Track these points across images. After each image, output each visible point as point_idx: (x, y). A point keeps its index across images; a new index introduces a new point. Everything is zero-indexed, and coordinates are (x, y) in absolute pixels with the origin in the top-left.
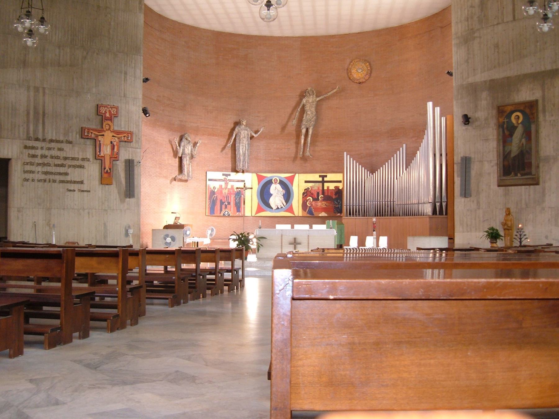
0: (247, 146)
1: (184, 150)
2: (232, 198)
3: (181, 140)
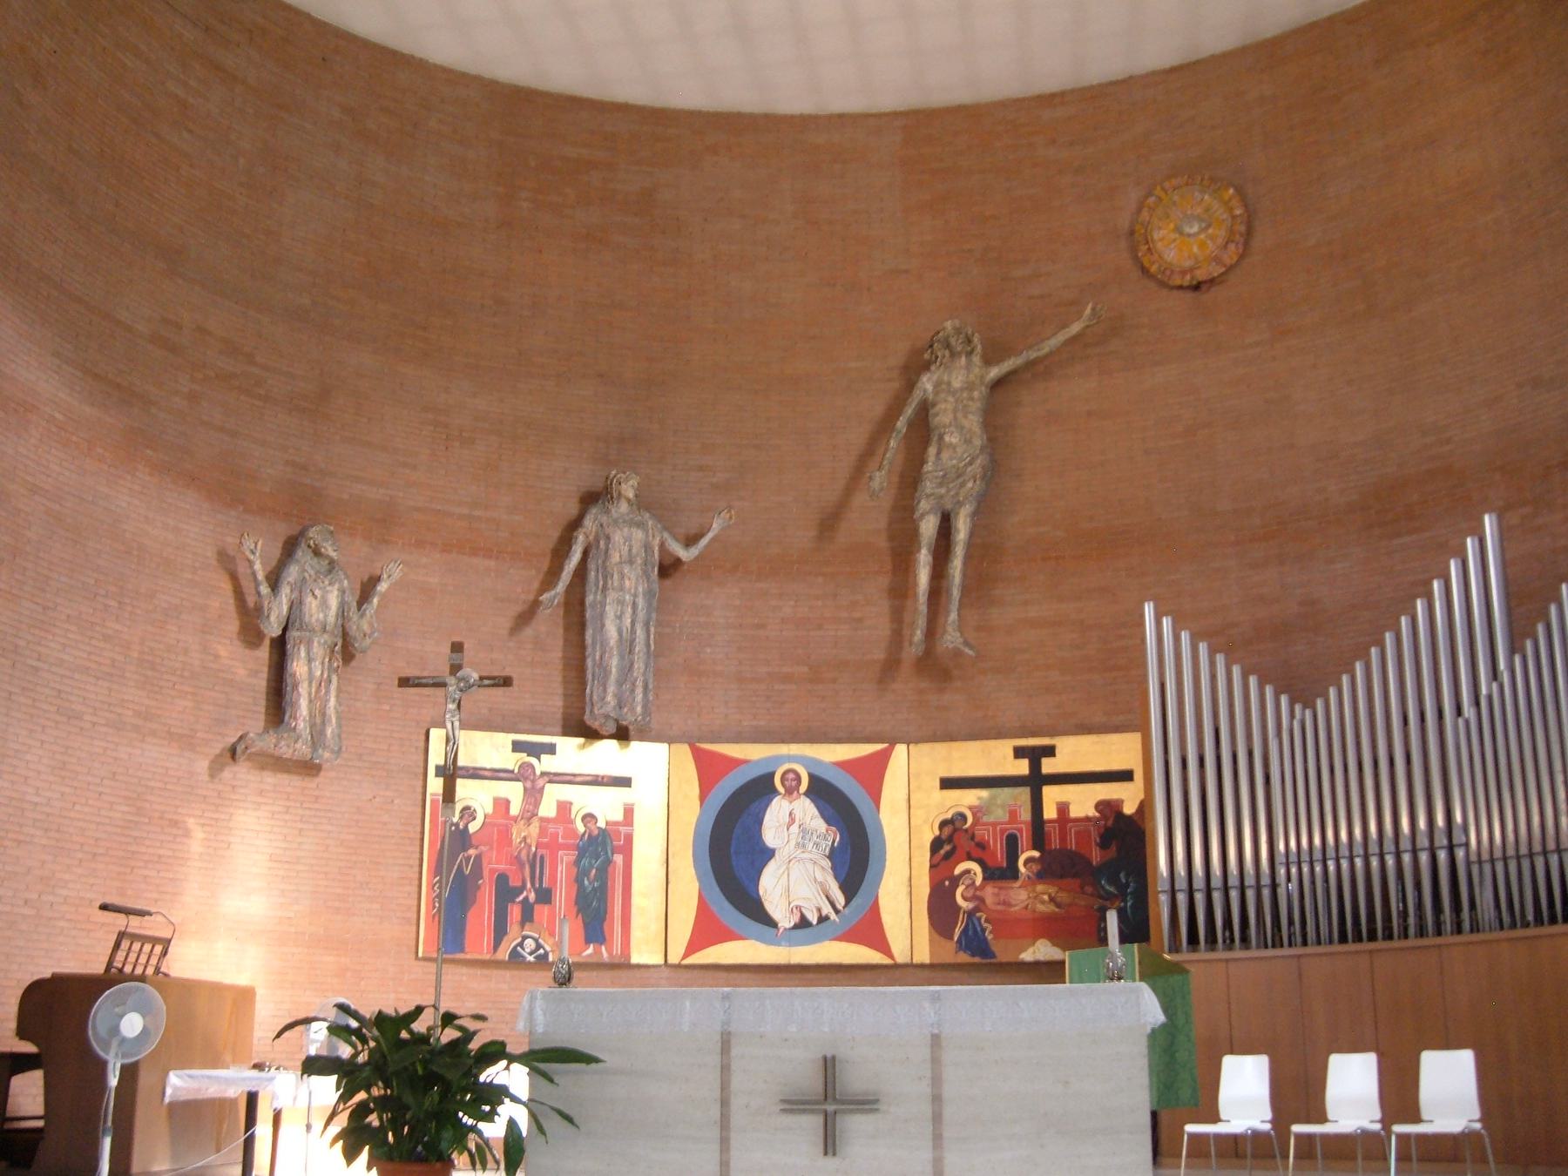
0: (641, 602)
1: (296, 606)
2: (562, 870)
3: (290, 548)
